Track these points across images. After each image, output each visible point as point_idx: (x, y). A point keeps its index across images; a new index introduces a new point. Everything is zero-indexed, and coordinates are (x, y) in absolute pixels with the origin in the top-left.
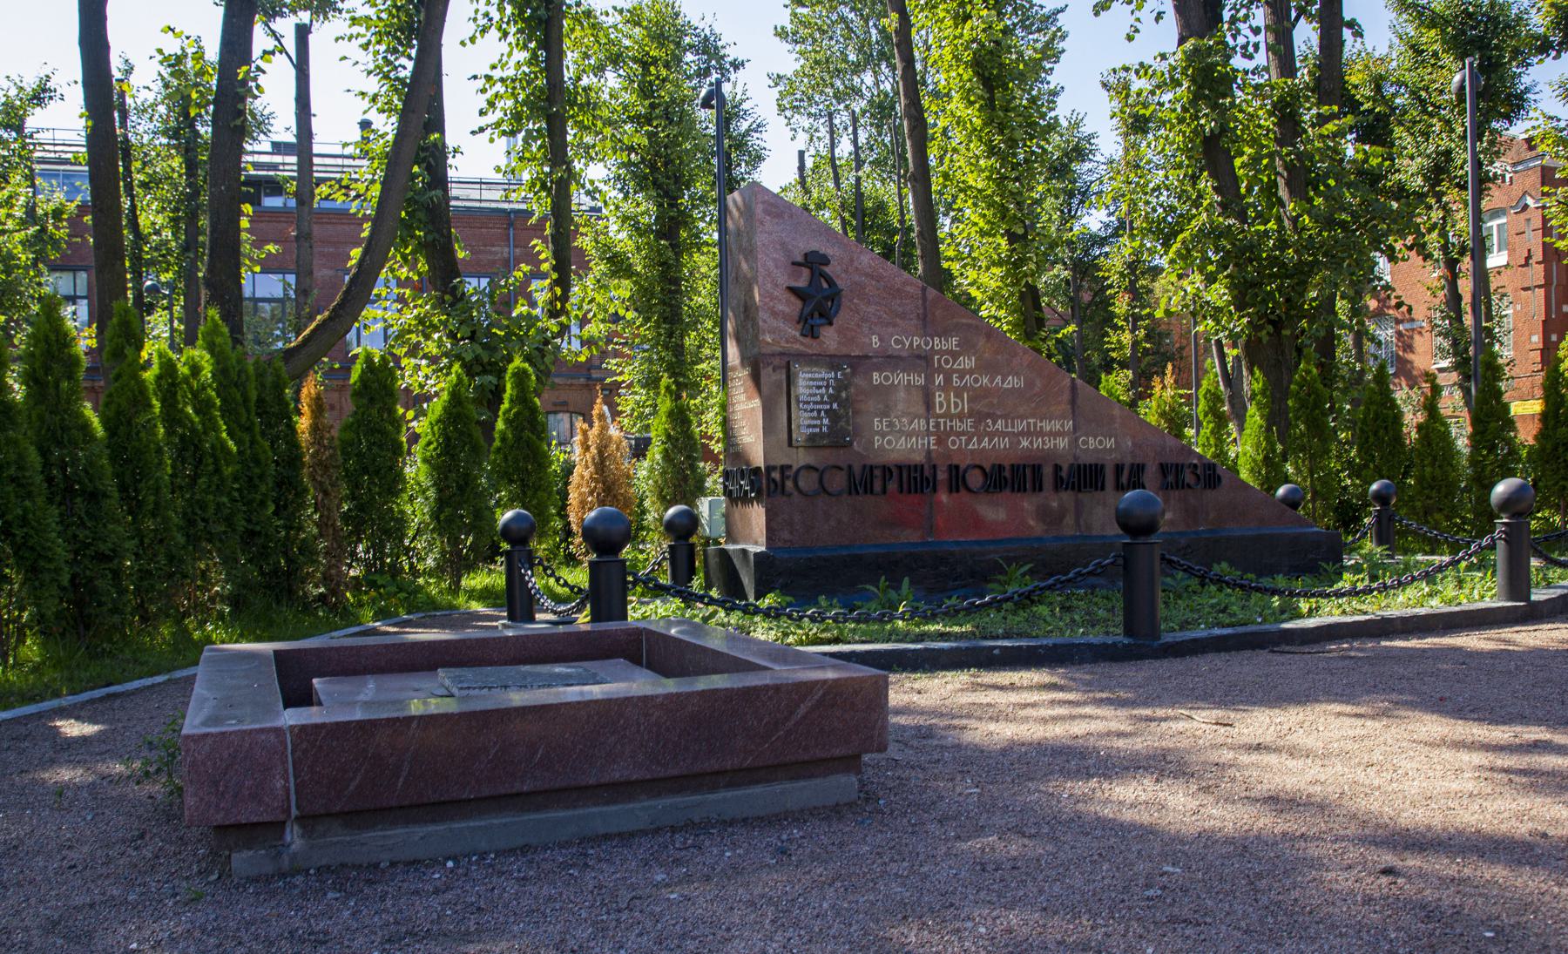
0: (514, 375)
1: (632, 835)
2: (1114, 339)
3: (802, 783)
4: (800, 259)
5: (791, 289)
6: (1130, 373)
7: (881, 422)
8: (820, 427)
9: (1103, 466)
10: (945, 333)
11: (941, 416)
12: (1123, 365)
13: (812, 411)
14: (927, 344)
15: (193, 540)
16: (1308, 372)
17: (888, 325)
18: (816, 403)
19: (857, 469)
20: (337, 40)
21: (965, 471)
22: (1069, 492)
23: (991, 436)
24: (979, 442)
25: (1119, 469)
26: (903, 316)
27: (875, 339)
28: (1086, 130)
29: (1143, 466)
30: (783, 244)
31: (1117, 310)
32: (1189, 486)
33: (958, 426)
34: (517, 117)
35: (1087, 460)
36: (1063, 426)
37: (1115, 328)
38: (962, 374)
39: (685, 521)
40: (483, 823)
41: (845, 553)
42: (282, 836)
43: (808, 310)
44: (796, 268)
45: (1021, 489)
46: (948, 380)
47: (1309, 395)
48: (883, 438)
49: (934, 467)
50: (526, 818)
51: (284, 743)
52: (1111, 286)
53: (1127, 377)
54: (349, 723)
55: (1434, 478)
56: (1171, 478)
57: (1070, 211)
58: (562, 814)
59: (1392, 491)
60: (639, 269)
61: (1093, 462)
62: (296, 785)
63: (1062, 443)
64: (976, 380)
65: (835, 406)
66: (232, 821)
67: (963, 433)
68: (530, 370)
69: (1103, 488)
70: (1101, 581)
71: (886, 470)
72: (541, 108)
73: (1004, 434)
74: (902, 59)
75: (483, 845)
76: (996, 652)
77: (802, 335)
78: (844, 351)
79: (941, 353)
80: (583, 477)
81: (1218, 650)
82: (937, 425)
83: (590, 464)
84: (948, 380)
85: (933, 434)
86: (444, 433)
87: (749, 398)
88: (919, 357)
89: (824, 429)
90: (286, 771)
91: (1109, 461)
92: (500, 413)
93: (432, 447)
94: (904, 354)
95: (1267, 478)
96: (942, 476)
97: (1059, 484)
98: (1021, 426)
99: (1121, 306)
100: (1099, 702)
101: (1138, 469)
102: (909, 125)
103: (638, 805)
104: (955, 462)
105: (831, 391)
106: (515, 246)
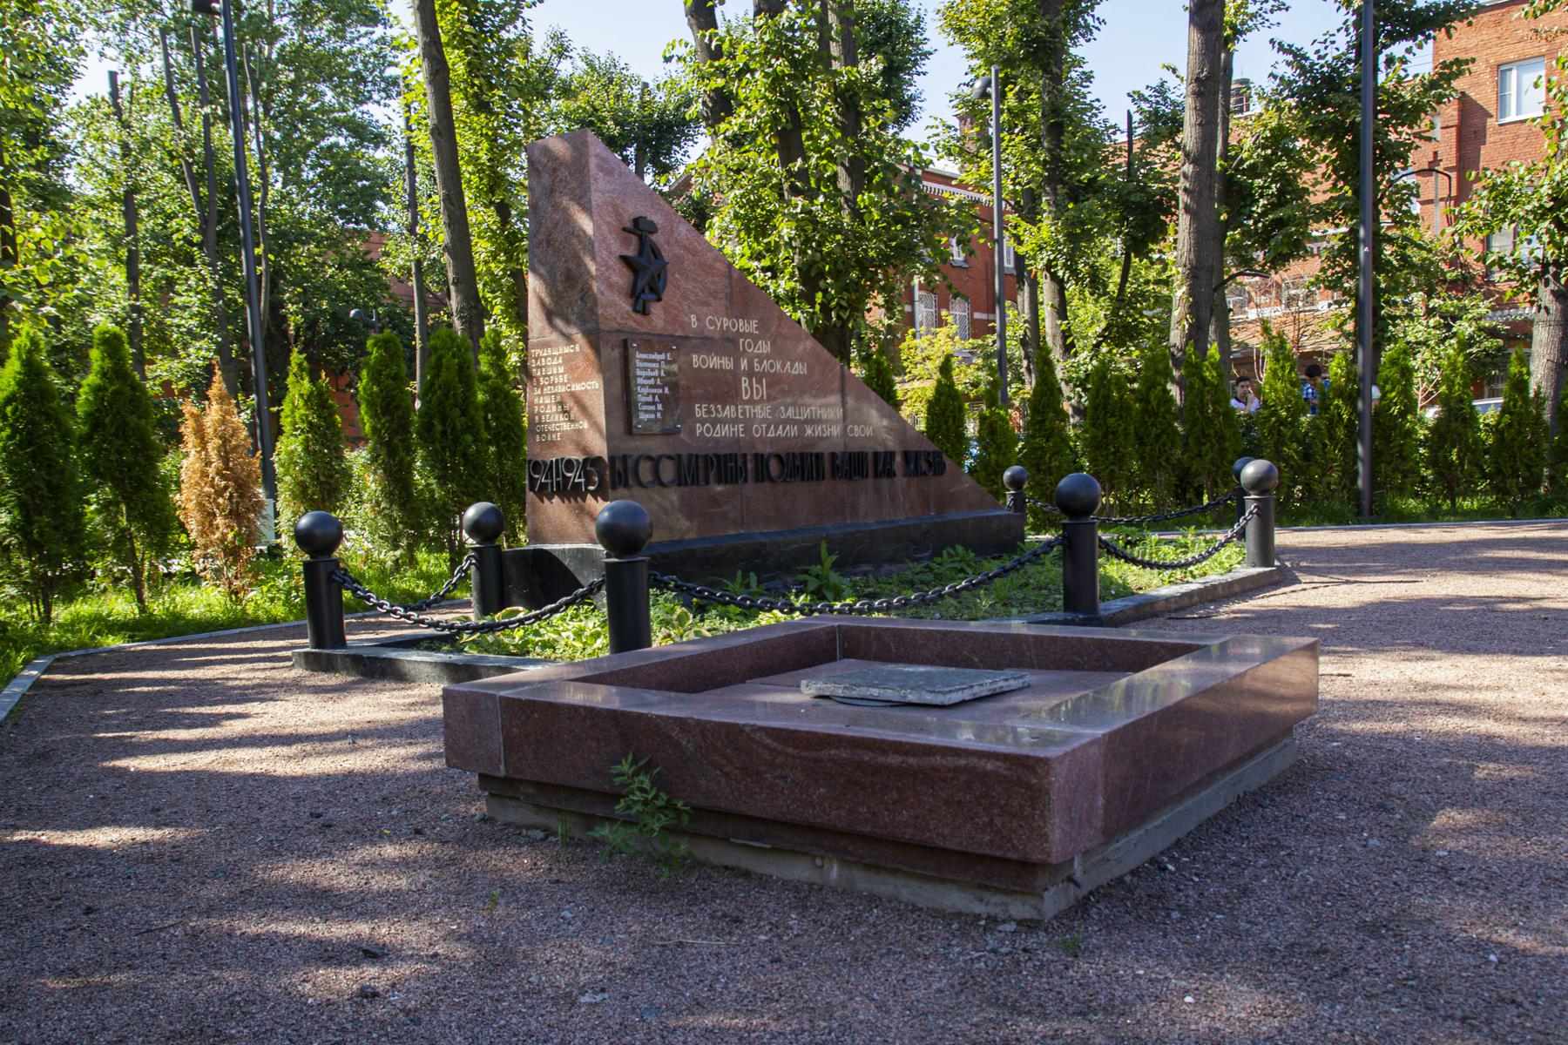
4: (629, 225)
5: (624, 259)
13: (648, 395)
14: (734, 327)
18: (651, 386)
19: (685, 459)
24: (776, 429)
27: (693, 318)
30: (614, 206)
35: (854, 448)
38: (761, 358)
44: (626, 234)
46: (751, 364)
63: (836, 431)
85: (740, 421)
88: (728, 339)
89: (659, 415)
104: (760, 451)
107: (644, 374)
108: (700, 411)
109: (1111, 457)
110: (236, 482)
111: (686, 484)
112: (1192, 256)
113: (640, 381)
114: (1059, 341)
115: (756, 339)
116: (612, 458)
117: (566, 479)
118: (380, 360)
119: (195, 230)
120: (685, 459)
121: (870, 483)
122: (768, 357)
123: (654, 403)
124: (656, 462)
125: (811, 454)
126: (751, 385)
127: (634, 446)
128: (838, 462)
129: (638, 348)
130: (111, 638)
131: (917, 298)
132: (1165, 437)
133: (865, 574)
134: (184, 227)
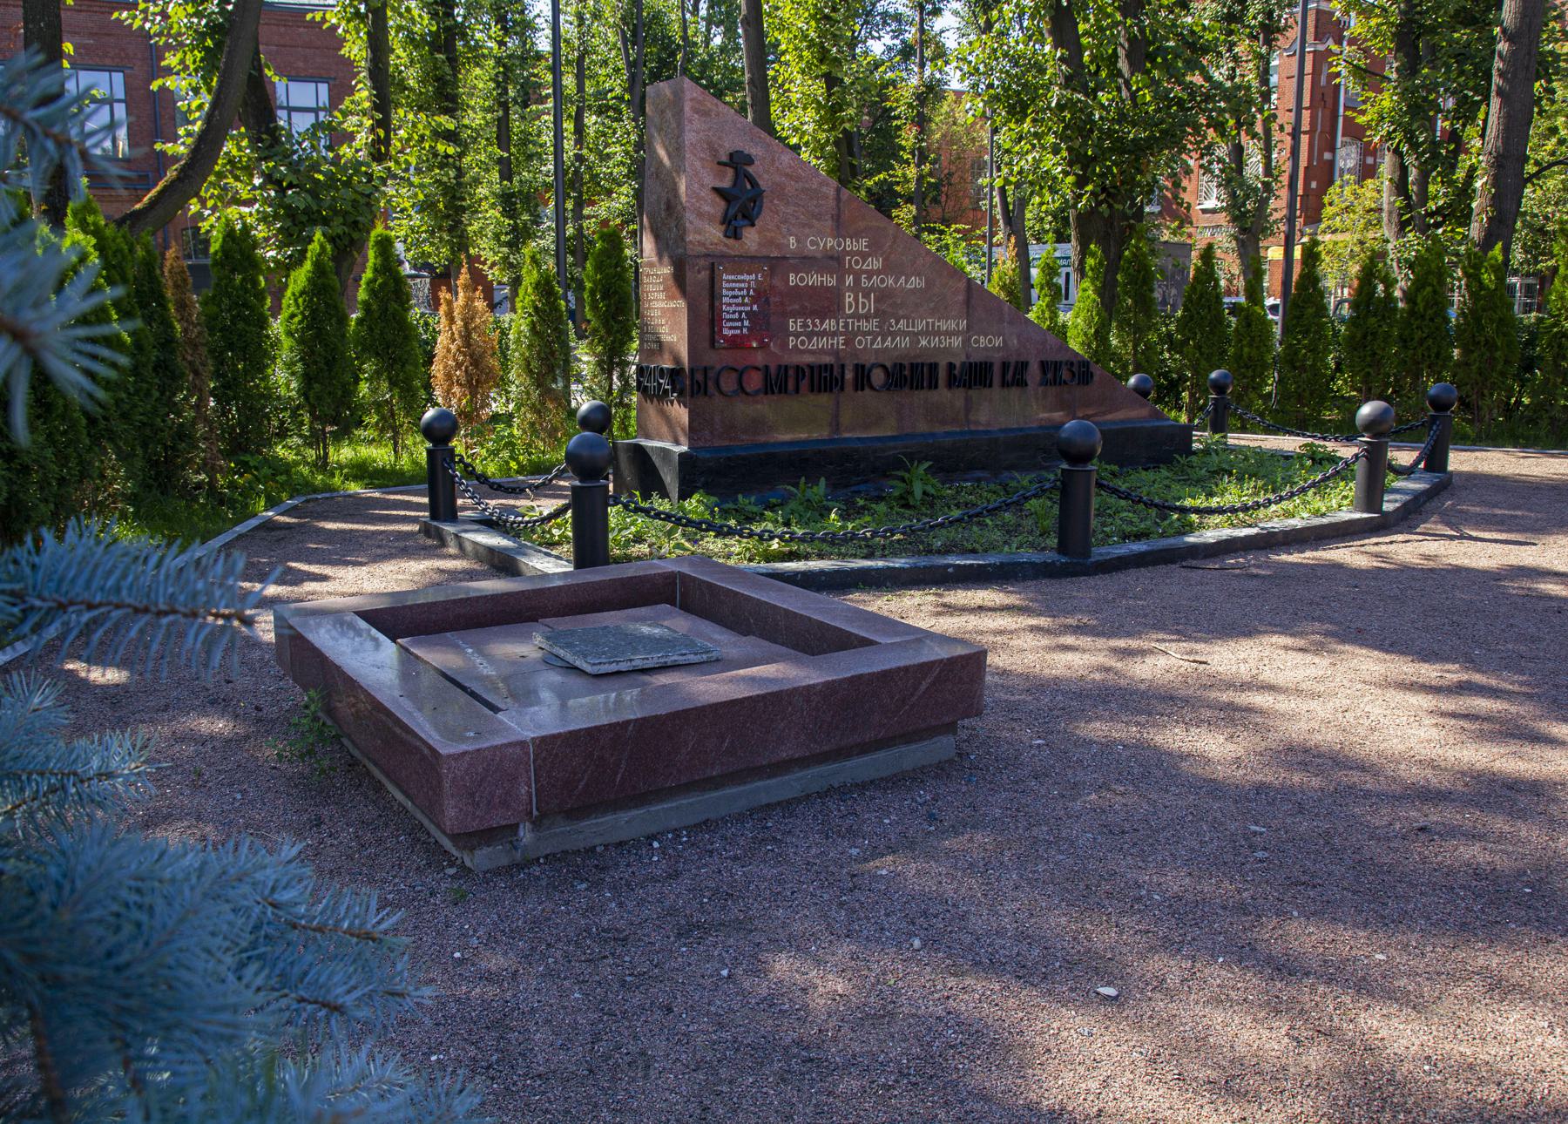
0: (377, 243)
1: (789, 802)
2: (899, 173)
3: (914, 746)
4: (724, 159)
5: (716, 190)
6: (913, 208)
7: (795, 322)
8: (741, 328)
9: (991, 364)
10: (856, 235)
11: (850, 316)
12: (909, 200)
13: (734, 312)
14: (839, 246)
15: (96, 440)
17: (804, 226)
18: (737, 305)
19: (773, 370)
21: (870, 371)
22: (961, 389)
23: (894, 335)
24: (883, 341)
25: (1005, 366)
26: (818, 217)
27: (792, 240)
29: (1027, 363)
30: (710, 143)
31: (903, 143)
32: (1065, 383)
33: (864, 325)
35: (976, 358)
36: (957, 325)
38: (870, 274)
39: (599, 416)
40: (674, 804)
42: (516, 834)
43: (732, 212)
44: (722, 168)
46: (857, 281)
47: (1139, 271)
48: (797, 339)
49: (843, 367)
50: (706, 796)
52: (898, 118)
54: (580, 730)
55: (1250, 358)
56: (1050, 376)
59: (1229, 381)
60: (411, 83)
61: (983, 360)
62: (537, 790)
63: (957, 342)
64: (882, 281)
65: (755, 308)
67: (869, 333)
69: (991, 386)
70: (986, 474)
75: (674, 824)
76: (950, 570)
77: (726, 236)
78: (764, 252)
80: (449, 351)
81: (1138, 566)
82: (846, 324)
83: (456, 336)
84: (857, 281)
85: (842, 334)
88: (832, 258)
89: (745, 331)
90: (530, 778)
91: (997, 358)
92: (363, 282)
93: (296, 320)
94: (819, 255)
95: (1096, 351)
96: (849, 376)
97: (952, 382)
100: (1078, 630)
101: (1023, 366)
104: (861, 362)
105: (751, 293)
107: (730, 293)
108: (794, 325)
109: (1368, 359)
110: (471, 357)
111: (773, 393)
112: (1499, 144)
113: (725, 300)
114: (1395, 219)
115: (864, 256)
116: (692, 370)
117: (660, 384)
118: (602, 251)
119: (625, 90)
120: (773, 370)
121: (996, 392)
122: (878, 272)
123: (740, 320)
124: (741, 374)
125: (923, 364)
126: (856, 300)
127: (712, 359)
128: (956, 372)
129: (726, 271)
130: (353, 484)
131: (1339, 144)
132: (1430, 341)
133: (979, 480)
134: (617, 86)
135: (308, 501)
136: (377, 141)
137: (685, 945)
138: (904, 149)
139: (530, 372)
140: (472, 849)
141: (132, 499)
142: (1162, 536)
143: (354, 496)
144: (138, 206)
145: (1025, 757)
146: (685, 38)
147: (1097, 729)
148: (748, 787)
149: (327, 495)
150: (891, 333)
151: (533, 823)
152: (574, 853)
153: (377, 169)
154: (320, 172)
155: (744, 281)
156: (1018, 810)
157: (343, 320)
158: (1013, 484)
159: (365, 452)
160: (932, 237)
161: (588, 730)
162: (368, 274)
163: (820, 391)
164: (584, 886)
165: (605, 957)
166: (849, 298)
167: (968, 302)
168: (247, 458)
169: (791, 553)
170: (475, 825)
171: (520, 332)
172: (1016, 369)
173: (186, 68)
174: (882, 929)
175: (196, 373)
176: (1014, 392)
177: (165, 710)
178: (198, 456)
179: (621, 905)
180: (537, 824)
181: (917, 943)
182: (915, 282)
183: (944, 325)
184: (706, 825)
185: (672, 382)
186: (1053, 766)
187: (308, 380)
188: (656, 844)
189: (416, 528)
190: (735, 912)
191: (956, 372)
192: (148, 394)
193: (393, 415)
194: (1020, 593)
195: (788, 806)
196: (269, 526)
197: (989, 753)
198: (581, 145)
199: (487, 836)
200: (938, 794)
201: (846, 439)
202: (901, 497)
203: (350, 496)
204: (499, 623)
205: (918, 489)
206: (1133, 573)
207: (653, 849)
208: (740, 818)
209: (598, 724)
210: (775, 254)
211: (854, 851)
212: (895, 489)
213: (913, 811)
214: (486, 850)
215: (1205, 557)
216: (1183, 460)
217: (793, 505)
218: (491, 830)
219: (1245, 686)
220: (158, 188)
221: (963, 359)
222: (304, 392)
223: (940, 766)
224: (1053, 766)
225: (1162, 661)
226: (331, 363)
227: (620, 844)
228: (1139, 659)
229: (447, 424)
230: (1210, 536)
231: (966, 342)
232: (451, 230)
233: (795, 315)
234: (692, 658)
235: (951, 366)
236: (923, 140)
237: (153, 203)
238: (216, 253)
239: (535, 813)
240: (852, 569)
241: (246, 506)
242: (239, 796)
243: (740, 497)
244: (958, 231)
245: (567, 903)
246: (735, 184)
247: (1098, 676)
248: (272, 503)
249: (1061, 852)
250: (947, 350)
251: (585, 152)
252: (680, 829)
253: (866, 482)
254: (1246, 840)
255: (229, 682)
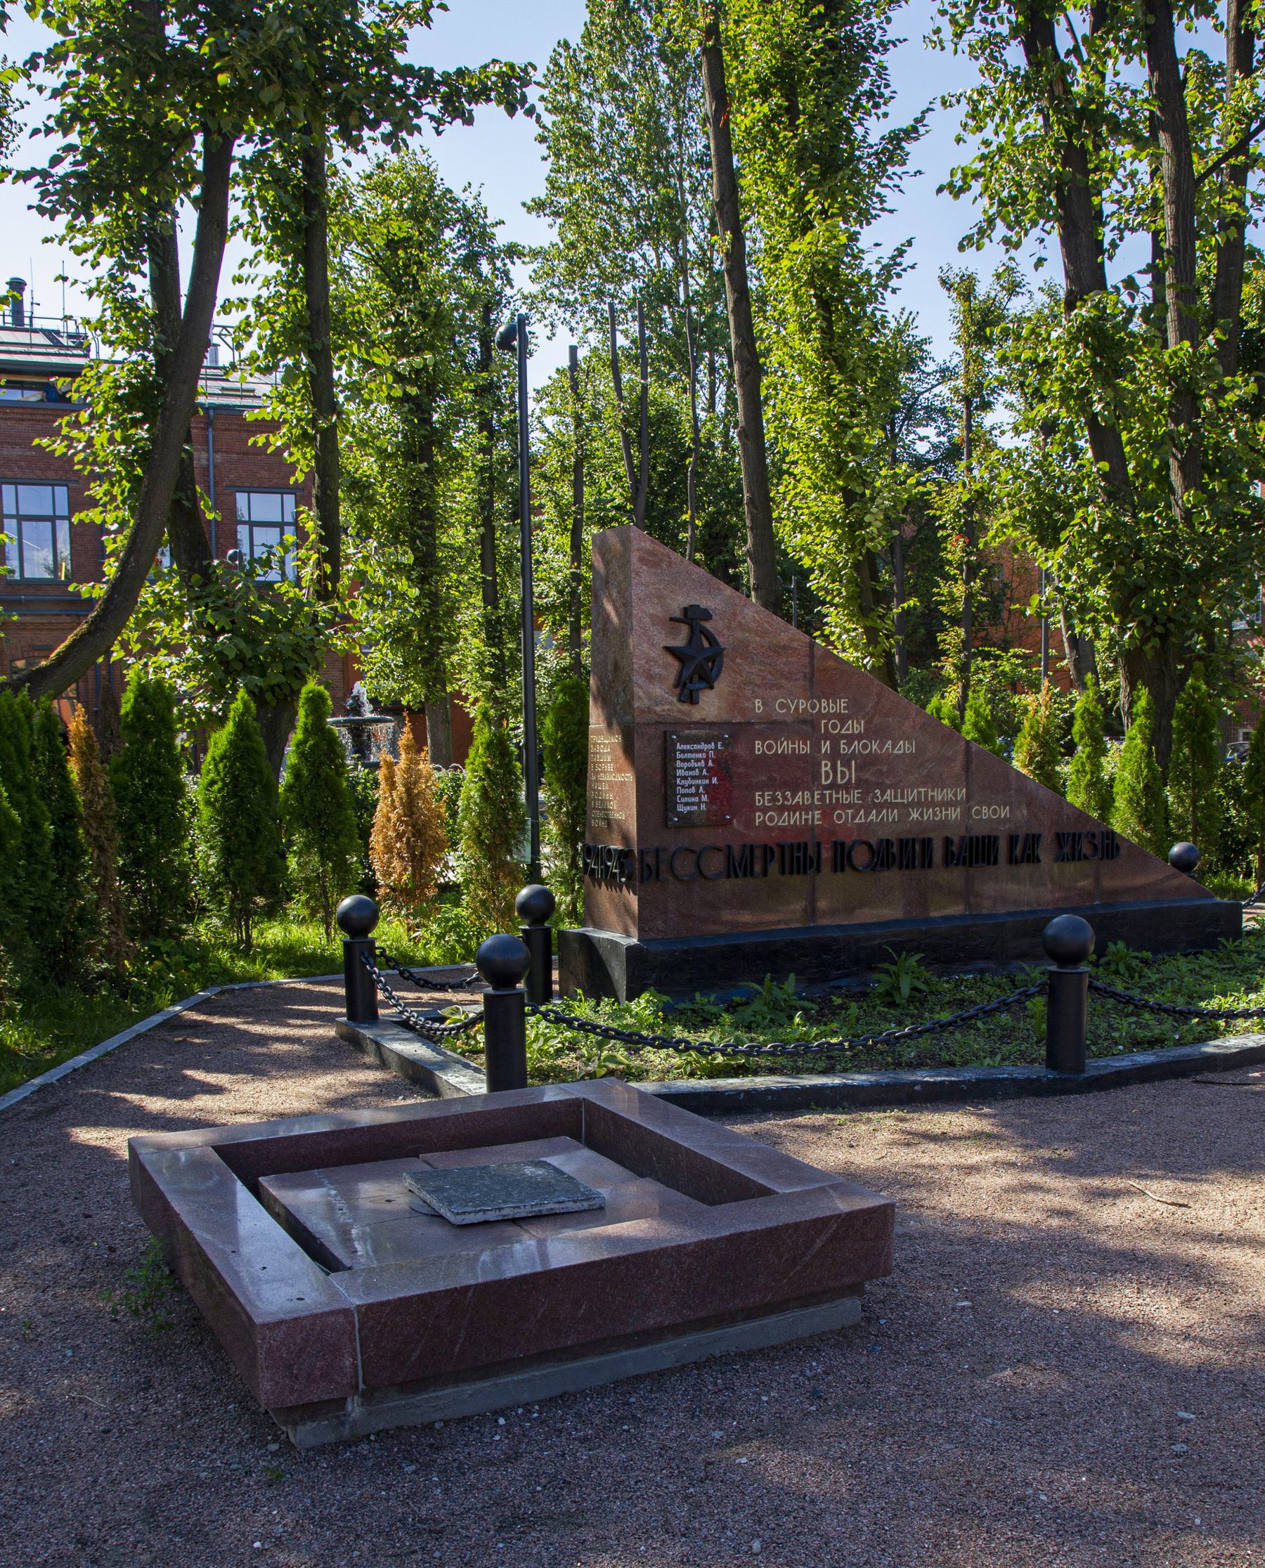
0: (308, 700)
1: (661, 1374)
2: (945, 591)
4: (678, 614)
5: (669, 650)
6: (962, 631)
9: (996, 839)
10: (832, 696)
14: (813, 707)
16: (1196, 689)
17: (772, 686)
18: (694, 778)
20: (46, 241)
22: (961, 867)
23: (880, 807)
24: (867, 814)
26: (788, 677)
27: (758, 703)
28: (920, 334)
29: (1039, 836)
31: (949, 556)
32: (1086, 857)
34: (273, 350)
36: (955, 795)
37: (947, 577)
38: (850, 739)
41: (723, 943)
42: (343, 1407)
43: (686, 674)
45: (910, 866)
46: (835, 746)
49: (819, 845)
50: (564, 1367)
51: (352, 1323)
52: (943, 527)
53: (958, 635)
54: (411, 1297)
56: (1067, 850)
57: (893, 429)
58: (596, 1360)
61: (985, 833)
63: (954, 814)
64: (865, 746)
65: (715, 780)
66: (306, 1400)
67: (849, 806)
68: (327, 693)
69: (995, 863)
70: (992, 965)
71: (767, 851)
72: (302, 341)
73: (891, 806)
74: (734, 290)
75: (526, 1397)
77: (680, 701)
79: (828, 716)
80: (389, 820)
81: (1142, 1081)
82: (823, 797)
83: (397, 804)
84: (835, 746)
85: (817, 808)
86: (230, 770)
87: (619, 770)
88: (805, 722)
89: (703, 807)
91: (1002, 832)
93: (216, 787)
94: (789, 719)
95: (1147, 809)
96: (826, 854)
97: (950, 858)
98: (911, 795)
99: (954, 550)
102: (741, 369)
103: (664, 1345)
104: (841, 838)
106: (215, 451)
107: (686, 765)
113: (679, 773)
115: (843, 719)
116: (641, 852)
119: (627, 499)
122: (859, 737)
123: (697, 794)
124: (699, 856)
126: (834, 768)
133: (982, 972)
135: (222, 993)
136: (324, 577)
137: (504, 1540)
138: (950, 563)
139: (482, 842)
140: (295, 1424)
141: (19, 994)
142: (1179, 1043)
143: (276, 987)
144: (44, 663)
145: (942, 1324)
146: (696, 440)
147: (1032, 1294)
148: (614, 1356)
149: (246, 985)
150: (875, 806)
151: (363, 1395)
152: (410, 1428)
153: (322, 609)
154: (258, 613)
155: (701, 751)
156: (916, 1388)
157: (270, 788)
158: (1020, 977)
159: (296, 932)
160: (987, 663)
161: (420, 1297)
162: (298, 735)
163: (792, 873)
164: (413, 1468)
165: (414, 1552)
166: (825, 767)
167: (967, 767)
168: (159, 943)
169: (740, 1067)
170: (292, 1400)
171: (469, 798)
172: (1026, 842)
173: (114, 498)
174: (725, 1528)
175: (102, 849)
176: (1025, 869)
177: (11, 1250)
178: (100, 942)
179: (447, 1491)
180: (368, 1397)
181: (756, 1545)
182: (904, 747)
183: (939, 795)
184: (563, 1399)
185: (621, 866)
186: (972, 1335)
187: (228, 853)
188: (502, 1421)
189: (331, 1032)
190: (568, 1504)
191: (954, 848)
192: (43, 875)
193: (325, 892)
194: (994, 1116)
195: (658, 1378)
196: (175, 1024)
197: (903, 1317)
198: (579, 561)
199: (310, 1410)
200: (832, 1366)
201: (823, 928)
202: (888, 994)
203: (271, 986)
204: (376, 1159)
205: (905, 985)
206: (1135, 1089)
207: (498, 1426)
208: (601, 1391)
209: (432, 1289)
210: (738, 719)
211: (717, 1434)
212: (879, 983)
213: (798, 1385)
214: (310, 1426)
215: (1226, 1069)
216: (1230, 945)
217: (757, 1005)
218: (312, 1405)
219: (1220, 1239)
220: (67, 643)
221: (962, 832)
222: (223, 868)
223: (842, 1332)
224: (972, 1335)
225: (1135, 1205)
226: (254, 835)
227: (464, 1419)
228: (1109, 1201)
229: (367, 913)
230: (1233, 1042)
231: (967, 813)
232: (426, 662)
233: (763, 787)
234: (572, 1206)
235: (948, 842)
236: (971, 554)
237: (62, 658)
238: (127, 714)
239: (361, 1386)
240: (803, 1087)
241: (150, 998)
242: (69, 1353)
243: (698, 995)
244: (1016, 656)
245: (389, 1488)
246: (690, 641)
247: (1055, 1222)
248: (181, 994)
249: (950, 1440)
250: (944, 824)
251: (584, 570)
252: (534, 1403)
253: (847, 975)
254: (1168, 1428)
255: (87, 1216)
